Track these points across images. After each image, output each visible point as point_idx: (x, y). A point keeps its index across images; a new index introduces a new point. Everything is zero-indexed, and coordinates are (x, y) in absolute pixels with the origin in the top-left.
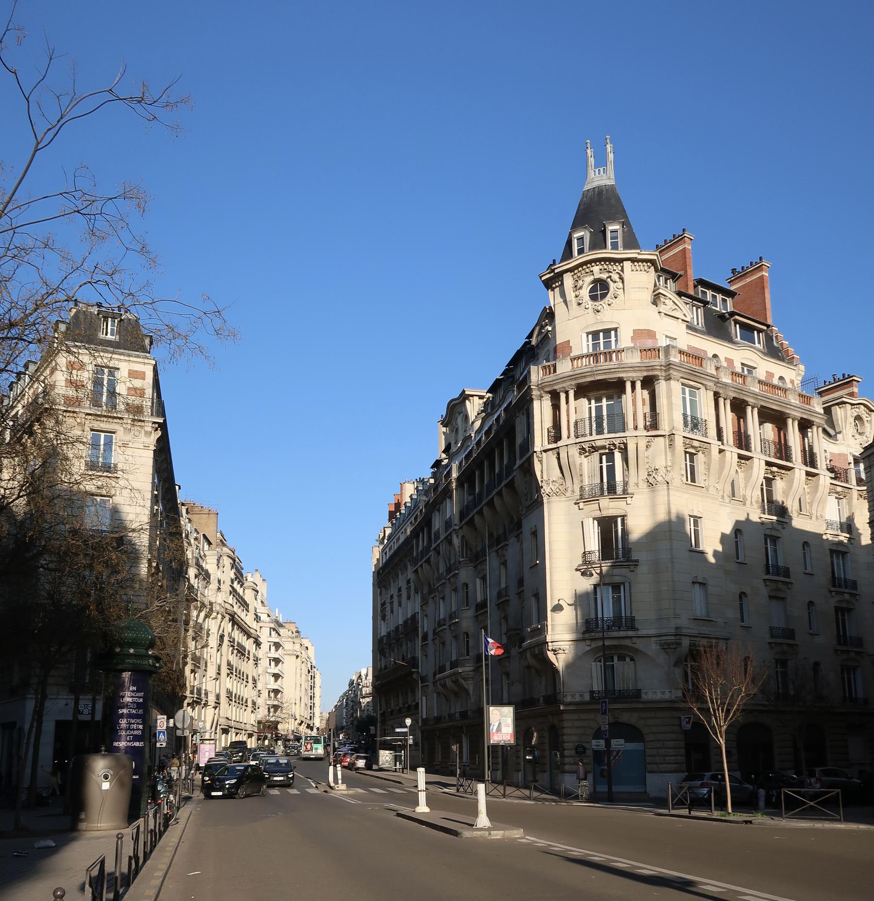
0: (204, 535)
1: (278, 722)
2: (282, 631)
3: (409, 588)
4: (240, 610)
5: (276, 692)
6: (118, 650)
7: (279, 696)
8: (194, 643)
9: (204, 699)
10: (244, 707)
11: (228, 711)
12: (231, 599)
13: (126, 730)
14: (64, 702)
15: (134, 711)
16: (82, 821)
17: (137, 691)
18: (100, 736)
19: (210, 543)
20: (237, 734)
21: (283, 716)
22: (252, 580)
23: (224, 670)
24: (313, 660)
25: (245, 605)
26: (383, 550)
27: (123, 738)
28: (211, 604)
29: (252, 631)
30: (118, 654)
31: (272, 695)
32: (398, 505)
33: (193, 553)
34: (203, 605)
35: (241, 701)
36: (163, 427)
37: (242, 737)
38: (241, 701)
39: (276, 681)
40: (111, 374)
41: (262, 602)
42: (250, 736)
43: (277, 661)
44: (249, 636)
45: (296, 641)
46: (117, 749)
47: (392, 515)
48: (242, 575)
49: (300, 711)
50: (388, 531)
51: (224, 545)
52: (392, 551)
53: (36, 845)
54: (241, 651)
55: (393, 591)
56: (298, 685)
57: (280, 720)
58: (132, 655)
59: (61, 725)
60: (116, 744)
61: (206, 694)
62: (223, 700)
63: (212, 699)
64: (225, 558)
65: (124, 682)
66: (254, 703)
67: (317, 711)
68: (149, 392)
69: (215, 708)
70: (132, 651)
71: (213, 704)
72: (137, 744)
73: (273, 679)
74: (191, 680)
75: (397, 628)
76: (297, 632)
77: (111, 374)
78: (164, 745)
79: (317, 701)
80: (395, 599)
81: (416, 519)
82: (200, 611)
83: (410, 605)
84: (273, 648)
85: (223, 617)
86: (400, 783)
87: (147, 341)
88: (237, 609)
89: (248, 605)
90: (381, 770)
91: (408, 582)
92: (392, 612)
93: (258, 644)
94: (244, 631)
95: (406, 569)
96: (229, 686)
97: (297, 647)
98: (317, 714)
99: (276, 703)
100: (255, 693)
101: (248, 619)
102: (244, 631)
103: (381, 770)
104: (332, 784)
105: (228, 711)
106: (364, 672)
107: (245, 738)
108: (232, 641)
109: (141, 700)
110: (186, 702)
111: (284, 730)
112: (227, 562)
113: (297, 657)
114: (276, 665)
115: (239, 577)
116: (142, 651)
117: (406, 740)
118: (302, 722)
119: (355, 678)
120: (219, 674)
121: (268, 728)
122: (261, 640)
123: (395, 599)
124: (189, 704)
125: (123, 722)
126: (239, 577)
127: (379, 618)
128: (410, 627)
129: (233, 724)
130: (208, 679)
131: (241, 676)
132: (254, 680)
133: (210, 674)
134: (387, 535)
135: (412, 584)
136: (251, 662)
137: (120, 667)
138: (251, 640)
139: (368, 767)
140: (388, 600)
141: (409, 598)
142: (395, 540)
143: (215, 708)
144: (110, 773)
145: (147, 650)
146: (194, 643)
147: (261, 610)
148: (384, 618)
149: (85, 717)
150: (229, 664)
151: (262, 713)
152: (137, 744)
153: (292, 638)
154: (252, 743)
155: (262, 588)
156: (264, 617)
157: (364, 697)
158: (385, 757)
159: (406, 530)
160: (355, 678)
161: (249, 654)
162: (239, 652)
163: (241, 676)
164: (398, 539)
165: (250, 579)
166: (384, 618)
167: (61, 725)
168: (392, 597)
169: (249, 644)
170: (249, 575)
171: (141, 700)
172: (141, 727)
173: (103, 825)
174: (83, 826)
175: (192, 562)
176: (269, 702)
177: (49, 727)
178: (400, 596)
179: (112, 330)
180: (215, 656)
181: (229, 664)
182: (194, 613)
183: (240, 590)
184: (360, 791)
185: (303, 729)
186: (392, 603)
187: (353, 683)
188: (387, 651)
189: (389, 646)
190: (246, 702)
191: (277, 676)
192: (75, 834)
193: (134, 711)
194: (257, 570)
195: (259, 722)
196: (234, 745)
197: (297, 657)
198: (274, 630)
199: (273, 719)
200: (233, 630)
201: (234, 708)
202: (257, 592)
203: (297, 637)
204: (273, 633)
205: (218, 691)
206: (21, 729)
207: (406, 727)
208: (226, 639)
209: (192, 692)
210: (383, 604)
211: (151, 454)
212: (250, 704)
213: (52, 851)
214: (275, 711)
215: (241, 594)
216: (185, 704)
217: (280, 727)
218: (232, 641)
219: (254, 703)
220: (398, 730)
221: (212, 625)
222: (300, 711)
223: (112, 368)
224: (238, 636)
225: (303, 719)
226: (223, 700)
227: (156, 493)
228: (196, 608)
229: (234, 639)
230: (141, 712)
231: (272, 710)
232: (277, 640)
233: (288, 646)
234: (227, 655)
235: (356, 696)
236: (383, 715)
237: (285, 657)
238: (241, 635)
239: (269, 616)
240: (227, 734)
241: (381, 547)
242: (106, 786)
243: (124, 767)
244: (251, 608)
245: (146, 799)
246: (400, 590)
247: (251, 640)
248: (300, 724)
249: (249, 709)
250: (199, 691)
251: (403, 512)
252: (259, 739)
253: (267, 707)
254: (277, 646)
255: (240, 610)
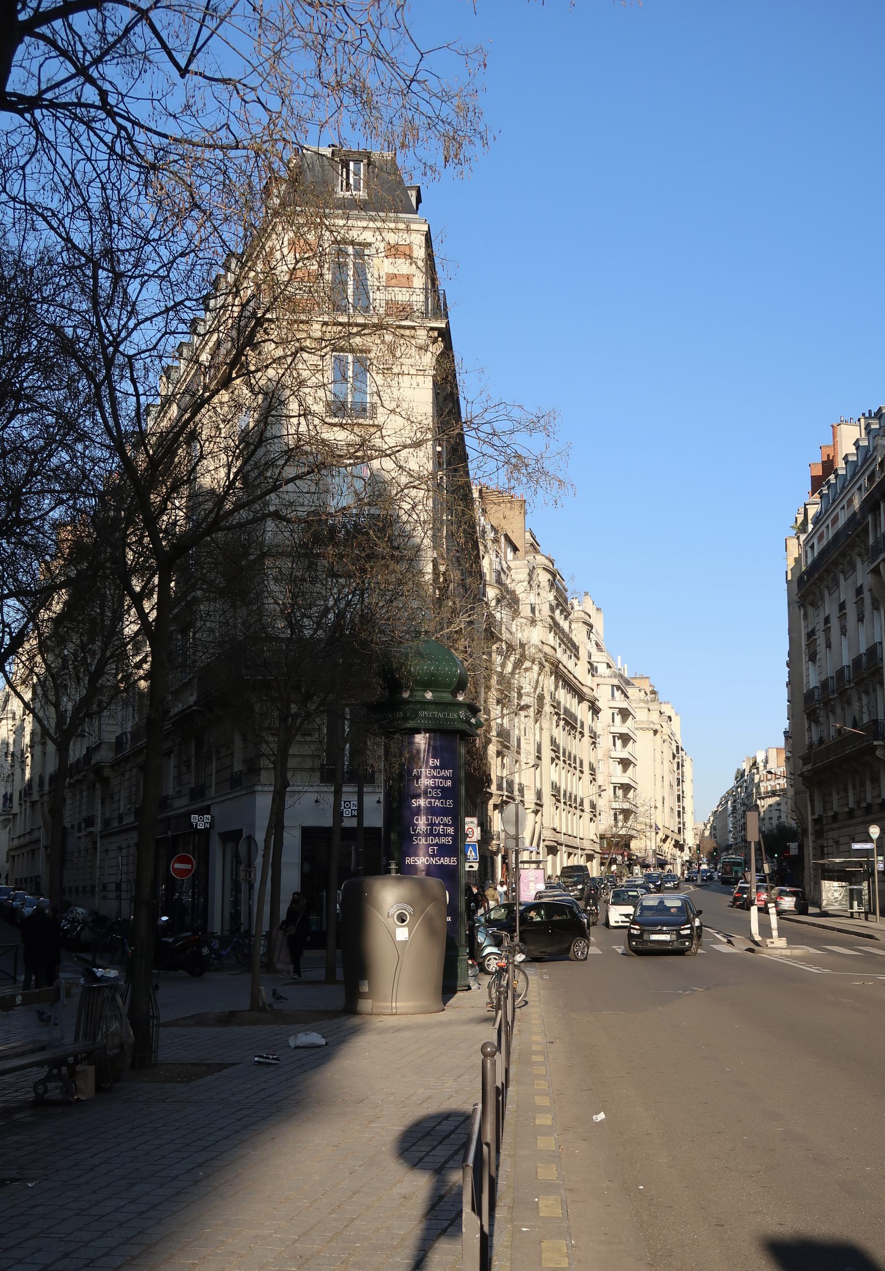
0: (507, 537)
1: (632, 837)
2: (630, 691)
3: (860, 603)
4: (566, 656)
5: (626, 788)
6: (406, 695)
7: (631, 795)
8: (499, 707)
9: (518, 798)
10: (578, 812)
11: (555, 818)
12: (551, 639)
13: (427, 836)
14: (314, 796)
15: (438, 803)
16: (363, 996)
17: (442, 767)
18: (384, 849)
19: (515, 549)
20: (570, 854)
21: (639, 827)
22: (581, 608)
23: (547, 754)
24: (678, 737)
25: (573, 648)
26: (806, 542)
27: (421, 852)
28: (522, 646)
29: (586, 690)
30: (406, 702)
31: (620, 793)
32: (828, 466)
33: (491, 564)
34: (510, 647)
35: (572, 803)
36: (445, 335)
37: (578, 860)
38: (572, 803)
39: (625, 770)
40: (359, 255)
41: (597, 644)
42: (590, 858)
43: (625, 739)
44: (581, 698)
45: (653, 706)
46: (413, 869)
47: (817, 483)
48: (566, 600)
49: (665, 819)
50: (812, 511)
51: (536, 551)
52: (824, 542)
53: (292, 1042)
54: (571, 723)
55: (830, 608)
56: (659, 779)
57: (633, 833)
58: (429, 703)
59: (309, 834)
60: (409, 861)
61: (521, 791)
62: (547, 799)
63: (530, 798)
64: (540, 571)
65: (418, 752)
66: (593, 806)
67: (688, 818)
68: (419, 281)
69: (536, 812)
70: (429, 695)
71: (533, 807)
72: (446, 861)
73: (620, 768)
74: (496, 769)
75: (840, 673)
76: (653, 692)
77: (359, 255)
78: (476, 867)
79: (688, 803)
80: (835, 624)
81: (871, 478)
82: (507, 657)
83: (863, 630)
84: (618, 718)
85: (542, 666)
86: (871, 937)
87: (413, 194)
88: (560, 655)
89: (577, 649)
90: (825, 914)
91: (859, 591)
92: (829, 645)
93: (595, 710)
94: (574, 690)
95: (854, 569)
96: (555, 777)
97: (655, 716)
98: (689, 825)
99: (626, 806)
100: (594, 789)
101: (579, 671)
102: (574, 690)
103: (825, 914)
104: (757, 938)
105: (555, 818)
106: (760, 758)
107: (582, 862)
108: (556, 705)
109: (449, 783)
110: (491, 803)
111: (640, 850)
112: (544, 578)
113: (655, 732)
114: (625, 745)
115: (562, 604)
116: (447, 696)
117: (871, 864)
118: (667, 837)
119: (745, 766)
120: (539, 758)
121: (616, 846)
122: (599, 704)
123: (835, 624)
124: (496, 807)
125: (421, 823)
126: (562, 604)
127: (805, 658)
128: (867, 670)
129: (562, 839)
130: (524, 766)
131: (571, 762)
132: (592, 769)
133: (525, 759)
134: (810, 516)
135: (867, 595)
136: (587, 739)
137: (411, 724)
138: (585, 705)
139: (801, 909)
140: (821, 626)
141: (861, 619)
142: (829, 522)
143: (536, 812)
144: (408, 911)
145: (454, 694)
146: (499, 707)
147: (597, 657)
148: (813, 658)
149: (350, 823)
150: (553, 741)
151: (605, 822)
152: (446, 861)
153: (647, 702)
154: (595, 870)
155: (597, 621)
156: (602, 669)
157: (763, 798)
158: (832, 892)
159: (850, 501)
160: (745, 766)
161: (582, 726)
162: (567, 723)
163: (571, 762)
164: (835, 520)
165: (576, 608)
166: (813, 658)
167: (309, 834)
168: (827, 620)
169: (581, 711)
170: (575, 602)
171: (449, 783)
172: (451, 830)
173: (401, 1005)
174: (366, 1005)
175: (490, 576)
176: (615, 805)
177: (292, 839)
178: (843, 617)
179: (357, 182)
180: (532, 733)
181: (553, 741)
182: (498, 659)
183: (565, 625)
184: (813, 951)
185: (668, 848)
186: (827, 631)
187: (743, 775)
188: (822, 713)
189: (826, 704)
190: (582, 804)
191: (625, 763)
192: (355, 1020)
193: (438, 803)
194: (586, 594)
195: (602, 837)
196: (568, 871)
197: (655, 732)
198: (619, 688)
199: (623, 832)
200: (556, 687)
201: (564, 814)
202: (591, 626)
203: (653, 701)
204: (617, 694)
205: (538, 786)
206: (250, 839)
207: (869, 839)
208: (547, 700)
209: (500, 788)
210: (811, 634)
211: (429, 383)
212: (587, 807)
213: (322, 1055)
214: (626, 819)
215: (566, 628)
216: (490, 807)
217: (634, 844)
218: (556, 705)
219: (593, 806)
220: (856, 846)
221: (528, 680)
222: (665, 819)
223: (360, 244)
224: (563, 696)
225: (669, 833)
226: (547, 799)
227: (439, 449)
228: (499, 652)
229: (559, 703)
230: (449, 804)
231: (621, 817)
232: (624, 705)
233: (641, 714)
234: (551, 729)
235: (749, 795)
236: (817, 821)
237: (636, 732)
238: (569, 696)
239: (609, 666)
240: (555, 855)
241: (803, 537)
242: (402, 934)
243: (434, 899)
244: (583, 653)
245: (464, 960)
246: (842, 606)
247: (585, 705)
248: (664, 841)
249: (587, 816)
250: (510, 784)
251: (842, 472)
252: (602, 864)
253: (612, 812)
254: (625, 714)
255: (566, 656)
